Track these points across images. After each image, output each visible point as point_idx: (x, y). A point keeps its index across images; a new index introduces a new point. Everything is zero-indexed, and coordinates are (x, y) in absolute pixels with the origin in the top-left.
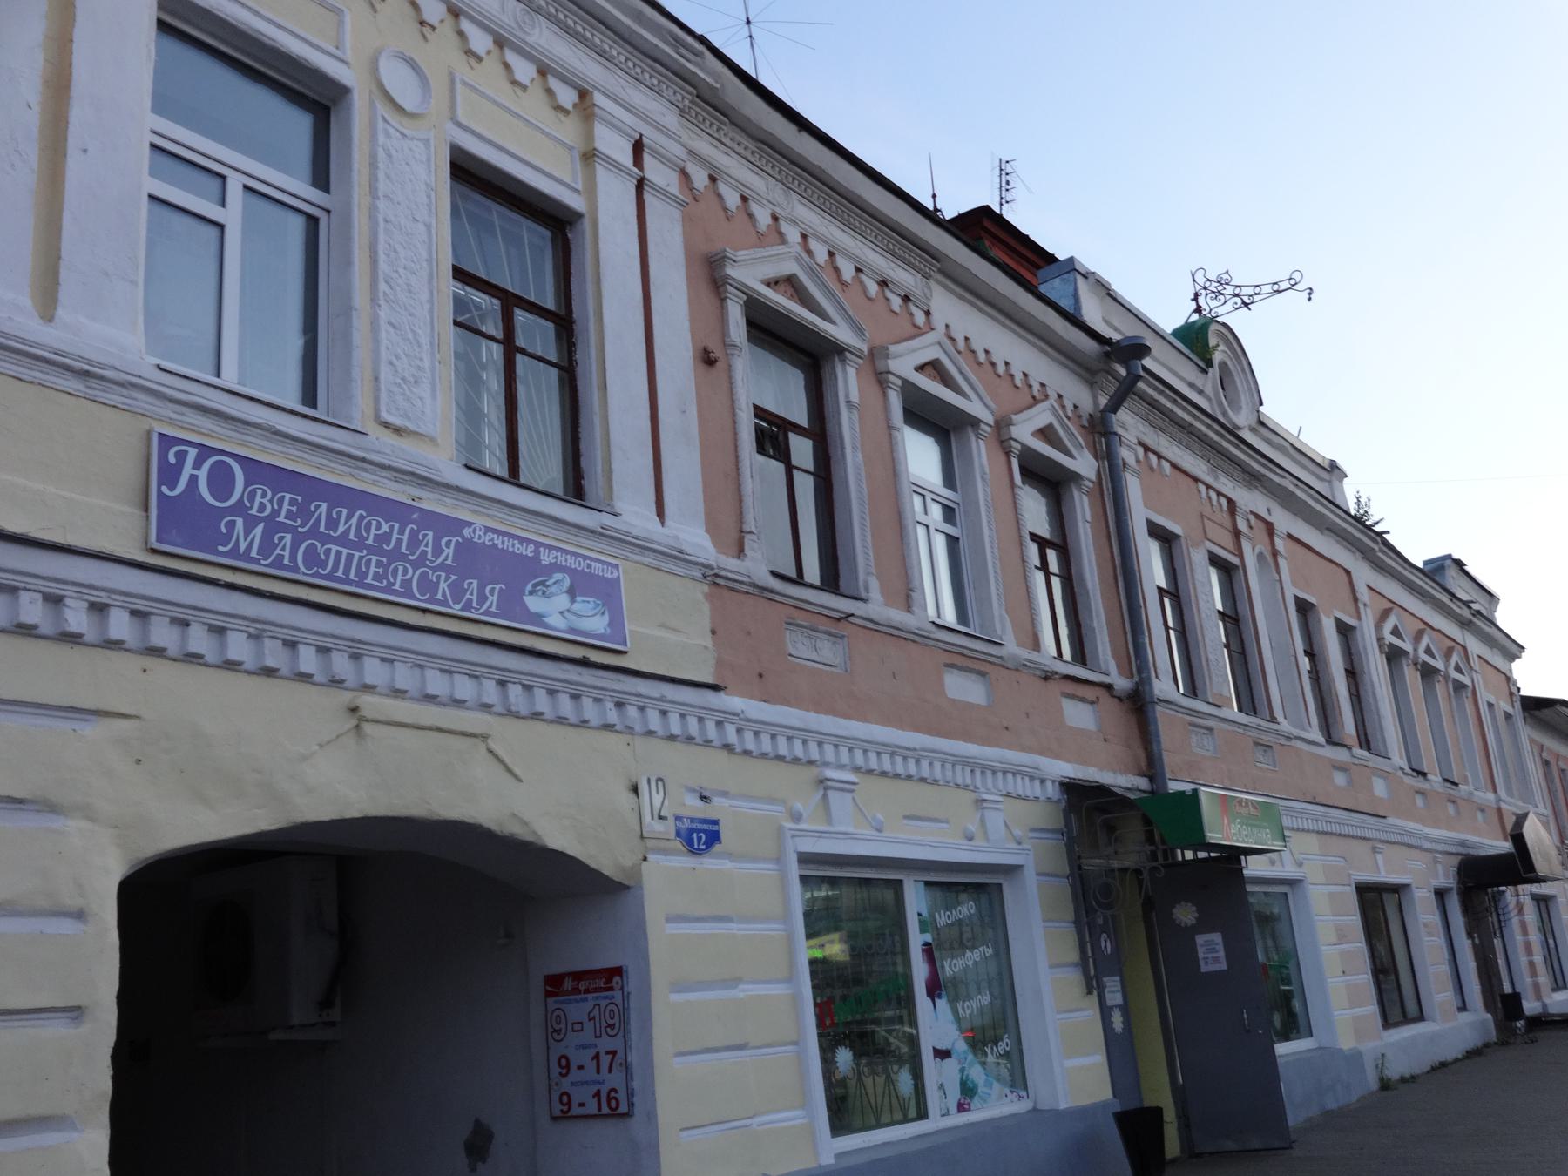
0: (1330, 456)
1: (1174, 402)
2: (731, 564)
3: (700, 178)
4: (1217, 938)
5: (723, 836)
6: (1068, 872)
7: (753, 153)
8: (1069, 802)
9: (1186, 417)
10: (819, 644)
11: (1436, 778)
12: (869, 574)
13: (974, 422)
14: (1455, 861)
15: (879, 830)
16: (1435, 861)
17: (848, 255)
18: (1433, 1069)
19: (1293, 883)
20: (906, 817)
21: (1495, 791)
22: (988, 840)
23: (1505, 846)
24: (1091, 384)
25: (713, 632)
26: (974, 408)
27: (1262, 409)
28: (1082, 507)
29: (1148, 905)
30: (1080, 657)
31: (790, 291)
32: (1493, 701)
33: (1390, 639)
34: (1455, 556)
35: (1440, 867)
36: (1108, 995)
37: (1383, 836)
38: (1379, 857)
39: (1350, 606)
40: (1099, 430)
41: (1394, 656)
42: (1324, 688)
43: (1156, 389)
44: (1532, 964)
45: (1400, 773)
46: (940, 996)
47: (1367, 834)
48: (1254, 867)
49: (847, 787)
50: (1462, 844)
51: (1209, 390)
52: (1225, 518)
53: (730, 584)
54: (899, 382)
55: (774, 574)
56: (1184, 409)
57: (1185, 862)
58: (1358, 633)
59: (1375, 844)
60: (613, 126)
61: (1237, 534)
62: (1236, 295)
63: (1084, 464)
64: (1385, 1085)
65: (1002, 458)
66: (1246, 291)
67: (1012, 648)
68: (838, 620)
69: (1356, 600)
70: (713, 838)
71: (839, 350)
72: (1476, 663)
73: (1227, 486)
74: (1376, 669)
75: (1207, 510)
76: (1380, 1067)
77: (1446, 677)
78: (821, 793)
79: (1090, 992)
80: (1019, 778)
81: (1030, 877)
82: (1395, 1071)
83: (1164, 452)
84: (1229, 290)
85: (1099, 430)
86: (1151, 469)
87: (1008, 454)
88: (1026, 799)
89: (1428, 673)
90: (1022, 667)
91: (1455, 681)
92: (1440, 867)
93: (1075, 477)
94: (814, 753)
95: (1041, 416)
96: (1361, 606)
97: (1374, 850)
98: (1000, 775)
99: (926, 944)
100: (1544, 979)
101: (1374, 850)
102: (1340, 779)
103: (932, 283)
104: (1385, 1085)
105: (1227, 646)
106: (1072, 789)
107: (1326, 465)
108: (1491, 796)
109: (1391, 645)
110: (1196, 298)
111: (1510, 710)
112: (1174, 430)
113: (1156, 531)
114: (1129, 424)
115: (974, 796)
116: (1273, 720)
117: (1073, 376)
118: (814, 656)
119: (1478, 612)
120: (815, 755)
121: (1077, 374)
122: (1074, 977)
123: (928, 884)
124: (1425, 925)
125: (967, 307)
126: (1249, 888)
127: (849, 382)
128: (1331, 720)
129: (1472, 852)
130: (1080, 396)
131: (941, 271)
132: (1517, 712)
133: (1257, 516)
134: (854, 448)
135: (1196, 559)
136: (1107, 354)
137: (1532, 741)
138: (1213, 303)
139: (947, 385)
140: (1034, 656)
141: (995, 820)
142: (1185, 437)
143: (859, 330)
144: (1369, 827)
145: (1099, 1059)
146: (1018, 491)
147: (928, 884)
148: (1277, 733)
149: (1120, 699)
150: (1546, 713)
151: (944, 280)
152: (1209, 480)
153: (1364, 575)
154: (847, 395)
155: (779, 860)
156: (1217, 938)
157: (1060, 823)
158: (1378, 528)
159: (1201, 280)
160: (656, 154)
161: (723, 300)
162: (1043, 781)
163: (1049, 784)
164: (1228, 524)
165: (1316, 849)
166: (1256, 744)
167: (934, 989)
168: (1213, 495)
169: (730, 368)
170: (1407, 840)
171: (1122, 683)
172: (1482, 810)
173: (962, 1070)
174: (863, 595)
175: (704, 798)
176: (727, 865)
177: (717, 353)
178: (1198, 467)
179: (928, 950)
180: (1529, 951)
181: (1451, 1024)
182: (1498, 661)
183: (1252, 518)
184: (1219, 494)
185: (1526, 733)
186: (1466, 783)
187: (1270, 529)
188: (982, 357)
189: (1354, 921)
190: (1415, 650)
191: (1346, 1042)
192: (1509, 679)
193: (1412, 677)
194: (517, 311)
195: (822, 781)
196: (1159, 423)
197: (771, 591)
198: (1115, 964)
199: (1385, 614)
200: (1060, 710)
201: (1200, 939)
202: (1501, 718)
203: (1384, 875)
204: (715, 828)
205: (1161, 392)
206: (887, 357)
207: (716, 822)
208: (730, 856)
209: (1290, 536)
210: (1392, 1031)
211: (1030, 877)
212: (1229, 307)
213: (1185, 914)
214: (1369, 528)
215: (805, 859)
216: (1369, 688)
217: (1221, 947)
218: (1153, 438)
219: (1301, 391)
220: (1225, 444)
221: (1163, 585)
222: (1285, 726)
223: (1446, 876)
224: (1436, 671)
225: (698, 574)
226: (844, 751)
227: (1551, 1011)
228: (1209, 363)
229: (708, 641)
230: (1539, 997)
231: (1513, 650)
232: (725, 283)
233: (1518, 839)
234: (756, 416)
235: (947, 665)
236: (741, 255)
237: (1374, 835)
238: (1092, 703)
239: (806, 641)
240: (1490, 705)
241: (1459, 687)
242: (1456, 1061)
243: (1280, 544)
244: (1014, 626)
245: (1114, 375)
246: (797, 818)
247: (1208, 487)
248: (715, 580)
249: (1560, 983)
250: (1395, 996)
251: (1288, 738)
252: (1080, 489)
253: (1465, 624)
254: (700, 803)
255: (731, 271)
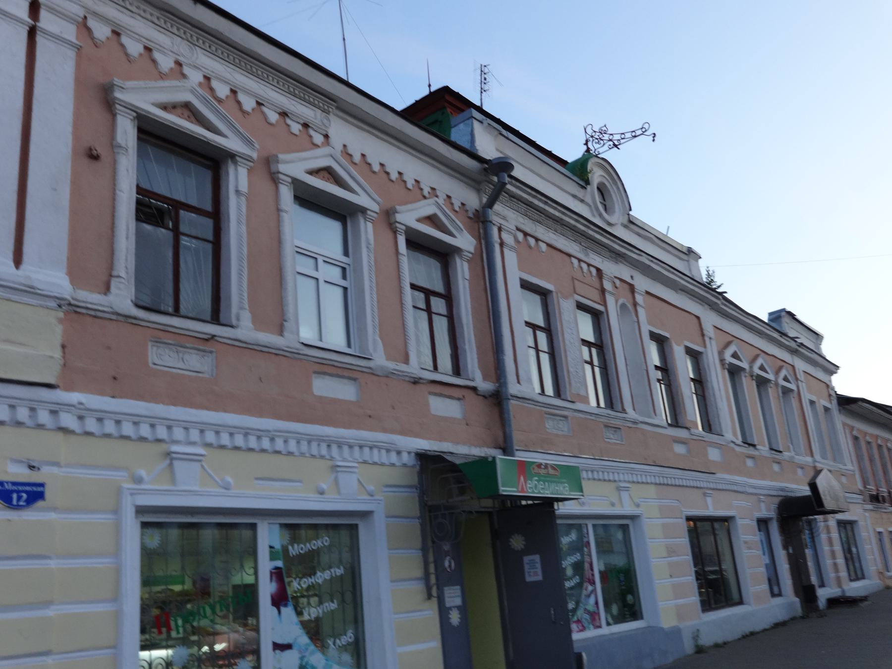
0: (687, 244)
1: (546, 203)
2: (91, 298)
3: (101, 32)
4: (537, 558)
5: (48, 494)
6: (419, 515)
7: (158, 18)
8: (421, 466)
9: (557, 214)
10: (186, 357)
11: (763, 449)
12: (242, 308)
13: (363, 210)
14: (777, 500)
15: (372, 496)
16: (760, 501)
17: (248, 92)
18: (745, 637)
19: (633, 518)
20: (257, 479)
21: (812, 455)
22: (339, 493)
23: (806, 491)
24: (478, 191)
25: (63, 347)
26: (361, 199)
27: (631, 213)
28: (462, 270)
29: (496, 535)
30: (457, 370)
31: (186, 113)
32: (814, 398)
33: (729, 359)
34: (788, 309)
35: (763, 505)
36: (447, 600)
37: (712, 486)
38: (709, 500)
39: (699, 339)
40: (480, 221)
41: (734, 372)
42: (674, 391)
43: (529, 194)
44: (835, 565)
45: (732, 445)
46: (286, 605)
47: (698, 484)
48: (562, 509)
49: (627, 489)
50: (782, 490)
51: (588, 199)
52: (595, 281)
53: (92, 313)
54: (289, 180)
55: (138, 306)
56: (555, 209)
57: (525, 506)
58: (704, 356)
59: (705, 492)
60: (65, 15)
61: (603, 291)
62: (611, 140)
63: (465, 241)
64: (700, 650)
65: (389, 235)
66: (617, 137)
67: (380, 360)
68: (207, 340)
69: (703, 335)
70: (40, 496)
71: (231, 156)
72: (801, 376)
73: (596, 260)
74: (718, 380)
75: (578, 275)
76: (696, 637)
77: (777, 384)
78: (168, 462)
79: (429, 596)
80: (375, 451)
81: (380, 522)
82: (706, 640)
83: (540, 236)
84: (606, 137)
85: (480, 221)
86: (530, 247)
87: (395, 232)
88: (383, 465)
89: (762, 383)
90: (389, 375)
91: (783, 387)
92: (763, 505)
93: (457, 250)
94: (162, 432)
95: (428, 208)
96: (707, 339)
97: (705, 495)
98: (357, 449)
99: (277, 568)
100: (844, 574)
101: (705, 495)
102: (680, 449)
103: (332, 117)
104: (700, 650)
105: (696, 394)
106: (424, 459)
107: (685, 250)
108: (809, 459)
109: (731, 364)
110: (586, 144)
111: (828, 405)
112: (550, 222)
113: (654, 337)
114: (506, 216)
115: (330, 463)
116: (624, 411)
117: (462, 184)
118: (180, 365)
119: (802, 344)
120: (617, 478)
121: (465, 183)
122: (418, 587)
123: (282, 526)
124: (746, 542)
125: (365, 135)
126: (559, 521)
127: (238, 179)
128: (678, 412)
129: (790, 494)
130: (473, 200)
131: (338, 108)
132: (834, 406)
133: (621, 280)
134: (239, 222)
135: (566, 308)
136: (485, 170)
137: (844, 425)
138: (597, 146)
139: (208, 130)
140: (403, 367)
141: (349, 482)
142: (559, 227)
143: (249, 142)
144: (701, 480)
145: (434, 645)
146: (286, 217)
147: (282, 526)
148: (624, 419)
149: (484, 397)
150: (853, 407)
151: (340, 114)
152: (581, 256)
153: (710, 319)
154: (237, 187)
155: (116, 511)
156: (537, 558)
157: (415, 480)
158: (719, 290)
159: (589, 131)
160: (52, 10)
161: (114, 115)
162: (399, 453)
163: (405, 456)
164: (598, 286)
165: (632, 495)
166: (606, 426)
167: (279, 600)
168: (584, 266)
169: (114, 164)
170: (735, 488)
171: (485, 386)
172: (802, 468)
173: (302, 658)
174: (234, 322)
175: (31, 467)
176: (53, 516)
177: (101, 149)
178: (572, 247)
179: (278, 575)
180: (833, 555)
181: (761, 604)
182: (821, 375)
183: (618, 282)
184: (589, 265)
185: (839, 419)
186: (789, 451)
187: (632, 288)
188: (376, 168)
189: (684, 541)
190: (751, 367)
191: (667, 622)
192: (828, 386)
193: (748, 386)
194: (182, 212)
195: (168, 454)
196: (536, 217)
197: (135, 318)
198: (457, 578)
199: (728, 344)
200: (427, 405)
201: (526, 559)
202: (821, 411)
203: (711, 509)
204: (40, 489)
205: (534, 197)
206: (278, 162)
207: (42, 485)
208: (54, 509)
209: (647, 293)
210: (711, 613)
211: (380, 522)
212: (606, 147)
213: (517, 542)
214: (714, 290)
215: (141, 510)
216: (711, 392)
217: (539, 566)
218: (529, 226)
219: (660, 199)
220: (591, 232)
221: (658, 364)
222: (631, 414)
223: (768, 510)
224: (768, 381)
225: (53, 304)
226: (304, 444)
227: (848, 594)
228: (588, 182)
229: (58, 354)
230: (839, 584)
231: (831, 369)
232: (114, 103)
233: (813, 486)
234: (137, 193)
235: (315, 372)
236: (129, 84)
237: (702, 485)
238: (459, 399)
239: (172, 354)
240: (812, 403)
241: (786, 391)
242: (765, 630)
243: (639, 299)
244: (384, 345)
245: (490, 182)
246: (139, 480)
247: (580, 260)
248: (72, 310)
249: (860, 575)
250: (716, 589)
251: (635, 423)
252: (461, 257)
253: (794, 352)
254: (27, 471)
255: (118, 95)
